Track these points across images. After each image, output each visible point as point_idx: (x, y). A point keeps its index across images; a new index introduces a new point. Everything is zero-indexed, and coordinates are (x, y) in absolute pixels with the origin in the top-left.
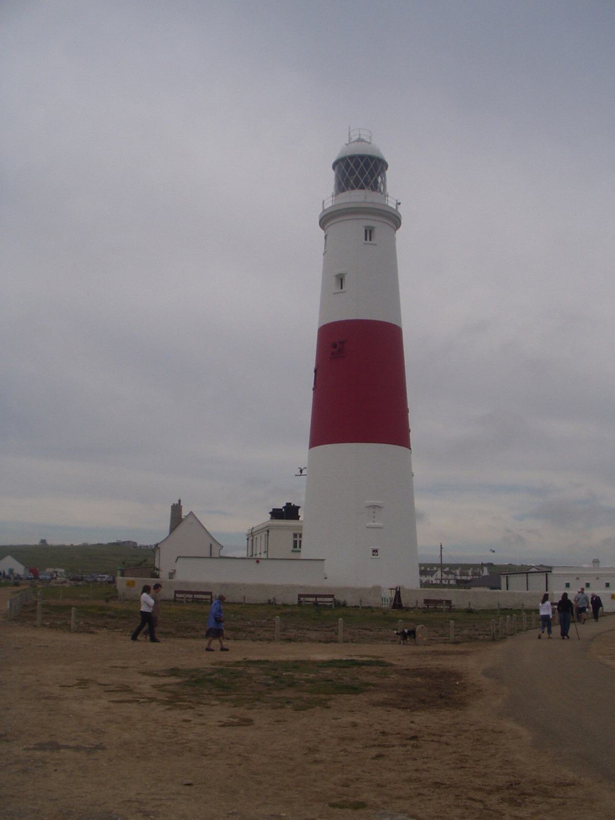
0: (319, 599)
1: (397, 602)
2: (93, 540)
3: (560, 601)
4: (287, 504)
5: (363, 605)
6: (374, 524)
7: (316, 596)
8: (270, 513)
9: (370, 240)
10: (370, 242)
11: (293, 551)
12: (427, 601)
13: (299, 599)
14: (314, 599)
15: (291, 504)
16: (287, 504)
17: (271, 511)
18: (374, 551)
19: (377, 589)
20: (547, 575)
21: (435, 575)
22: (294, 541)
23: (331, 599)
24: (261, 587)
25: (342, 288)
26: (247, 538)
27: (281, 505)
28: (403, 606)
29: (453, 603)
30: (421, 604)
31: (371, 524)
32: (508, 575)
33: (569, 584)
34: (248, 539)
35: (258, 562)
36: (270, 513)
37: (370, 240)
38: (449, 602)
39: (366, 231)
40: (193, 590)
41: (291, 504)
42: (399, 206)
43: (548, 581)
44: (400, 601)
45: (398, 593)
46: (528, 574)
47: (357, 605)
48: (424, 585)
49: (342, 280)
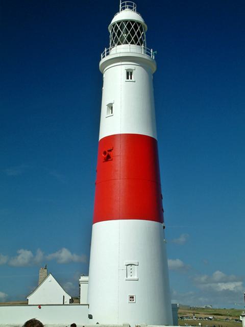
9: (131, 79)
10: (131, 80)
31: (129, 277)
39: (128, 73)
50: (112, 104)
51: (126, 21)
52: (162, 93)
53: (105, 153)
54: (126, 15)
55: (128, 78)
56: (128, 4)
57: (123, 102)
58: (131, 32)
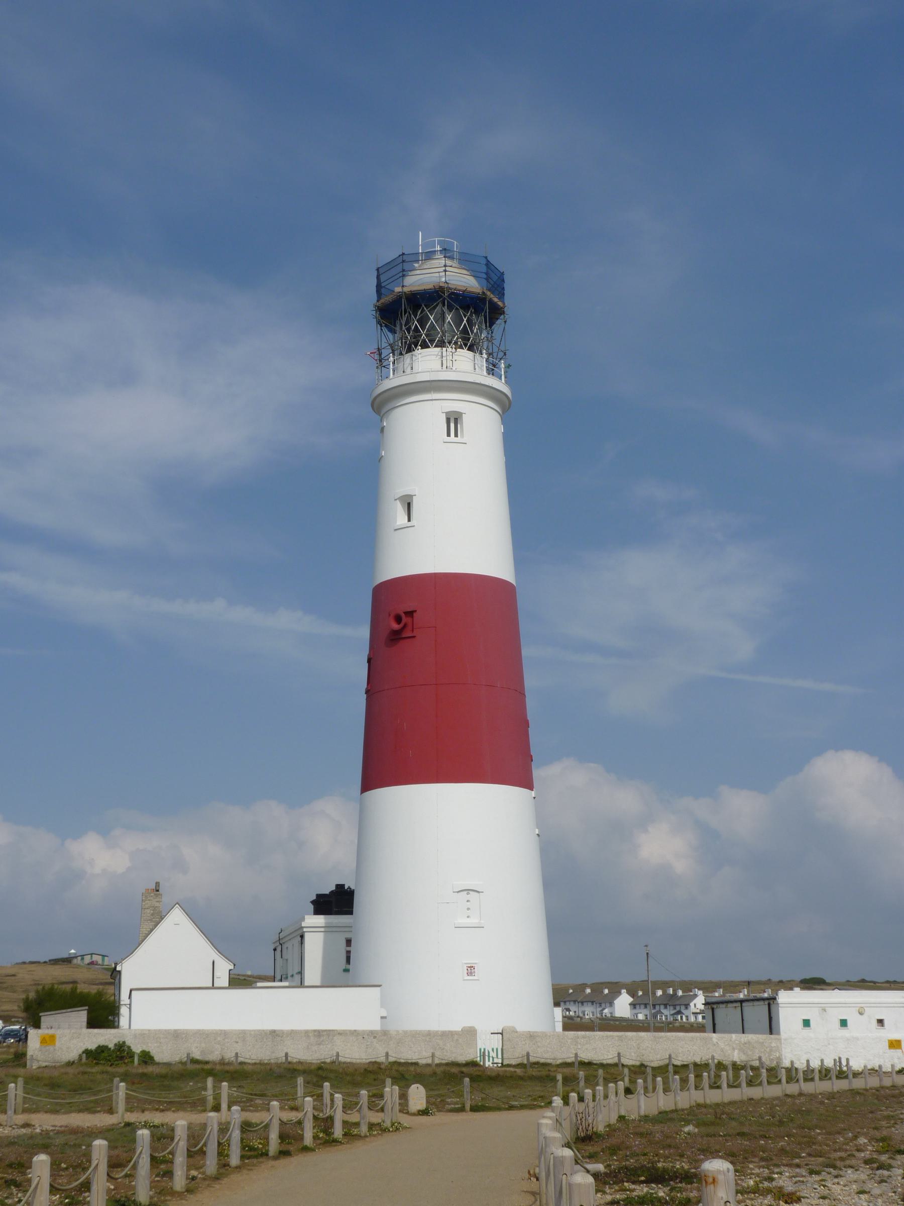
4: (337, 886)
5: (863, 1080)
6: (468, 920)
8: (313, 902)
9: (456, 435)
10: (456, 440)
15: (344, 885)
16: (337, 886)
17: (315, 898)
19: (470, 1033)
20: (769, 1005)
21: (692, 1004)
24: (176, 1035)
25: (409, 520)
26: (273, 948)
27: (328, 888)
32: (715, 1006)
34: (275, 950)
36: (313, 902)
37: (456, 435)
41: (344, 885)
42: (82, 1016)
43: (716, 1022)
45: (808, 1061)
46: (744, 1004)
47: (378, 1060)
48: (570, 1025)
49: (409, 505)
50: (411, 496)
53: (398, 619)
55: (449, 435)
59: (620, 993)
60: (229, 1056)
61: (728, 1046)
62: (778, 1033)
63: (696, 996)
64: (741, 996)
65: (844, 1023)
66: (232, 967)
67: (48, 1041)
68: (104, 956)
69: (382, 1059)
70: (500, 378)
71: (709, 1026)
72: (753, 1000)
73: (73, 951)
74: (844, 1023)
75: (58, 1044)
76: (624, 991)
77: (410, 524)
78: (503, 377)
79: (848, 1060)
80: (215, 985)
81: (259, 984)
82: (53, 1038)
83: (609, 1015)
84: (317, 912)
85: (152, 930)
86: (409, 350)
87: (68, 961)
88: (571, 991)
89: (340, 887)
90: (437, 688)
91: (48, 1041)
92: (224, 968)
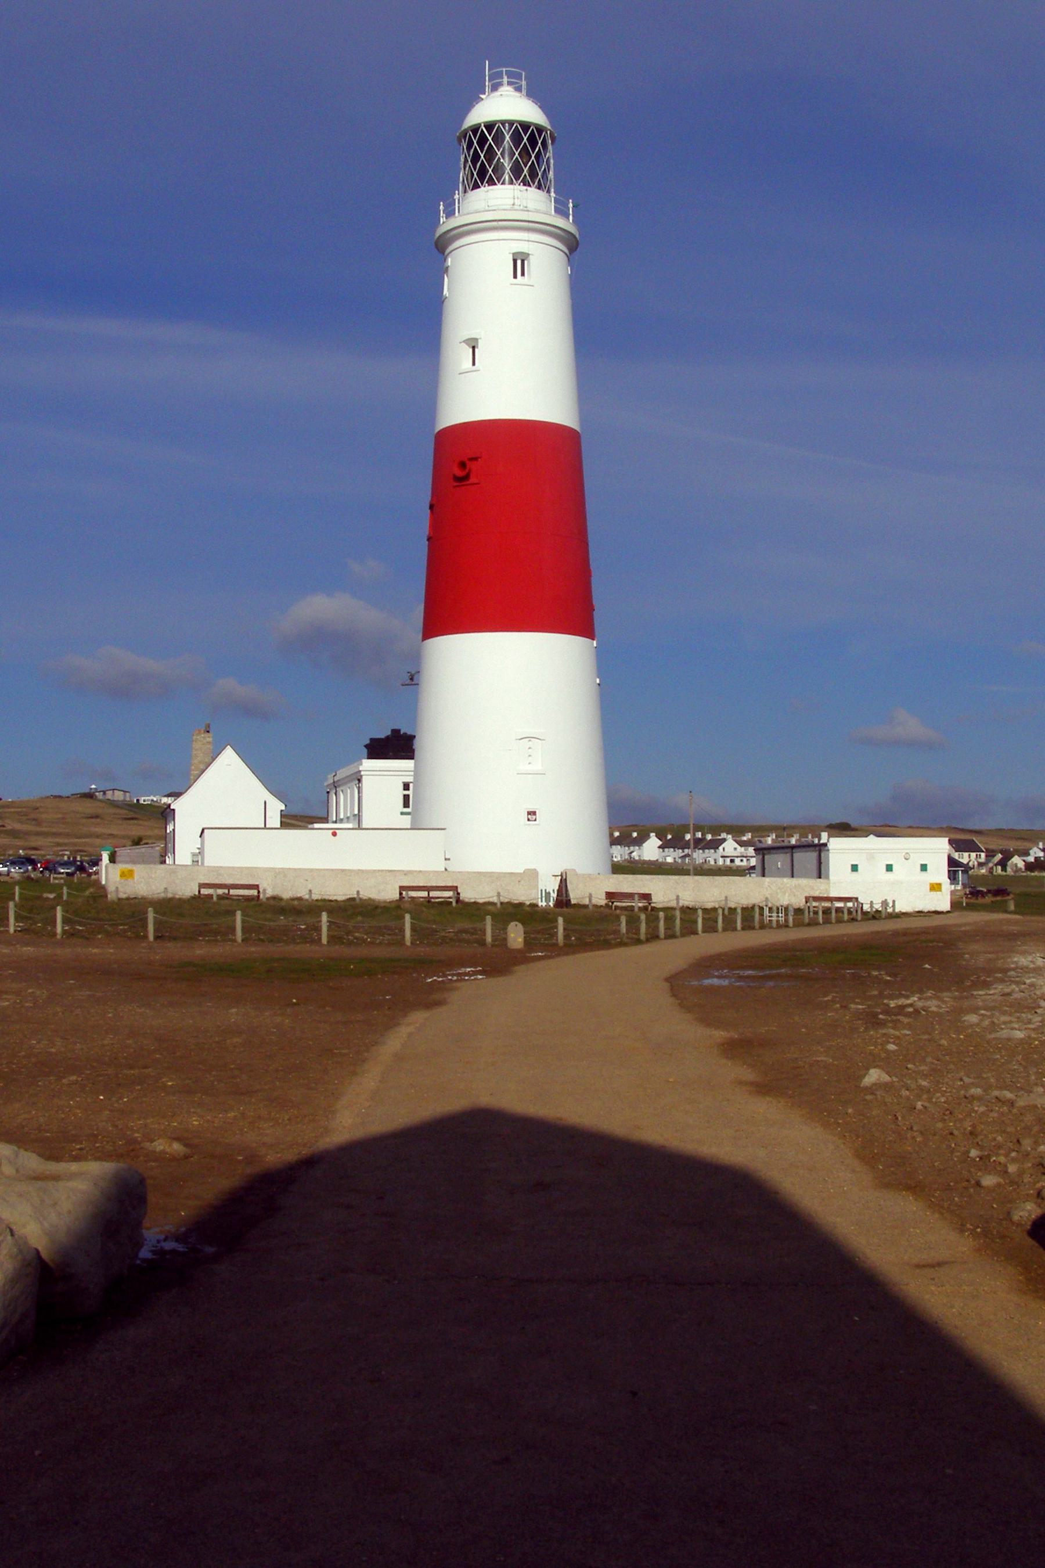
0: (433, 894)
1: (563, 900)
2: (574, 379)
3: (274, 898)
4: (393, 731)
7: (428, 889)
8: (366, 746)
9: (523, 274)
11: (402, 813)
12: (610, 895)
13: (401, 894)
14: (425, 894)
15: (399, 731)
16: (393, 731)
17: (368, 742)
18: (529, 813)
19: (532, 875)
21: (721, 848)
22: (284, 825)
23: (450, 894)
25: (474, 364)
28: (573, 902)
29: (654, 899)
30: (601, 900)
33: (857, 865)
35: (334, 834)
36: (366, 746)
37: (523, 274)
38: (647, 897)
40: (230, 881)
41: (399, 731)
44: (567, 895)
45: (310, 891)
47: (491, 900)
50: (476, 340)
51: (490, 126)
52: (597, 328)
53: (462, 465)
54: (506, 105)
55: (515, 277)
56: (510, 75)
57: (507, 341)
58: (526, 152)
59: (648, 837)
60: (303, 893)
61: (783, 890)
62: (827, 877)
63: (724, 840)
64: (793, 841)
65: (889, 868)
66: (283, 807)
67: (126, 875)
68: (125, 792)
69: (495, 900)
70: (568, 218)
71: (759, 869)
72: (804, 846)
73: (93, 786)
74: (889, 868)
75: (136, 877)
76: (653, 835)
77: (474, 368)
78: (571, 217)
79: (894, 902)
80: (815, 855)
81: (316, 826)
82: (131, 873)
83: (637, 858)
84: (371, 756)
85: (203, 771)
86: (476, 186)
87: (90, 796)
88: (635, 835)
89: (396, 732)
90: (504, 533)
91: (126, 875)
92: (276, 807)
